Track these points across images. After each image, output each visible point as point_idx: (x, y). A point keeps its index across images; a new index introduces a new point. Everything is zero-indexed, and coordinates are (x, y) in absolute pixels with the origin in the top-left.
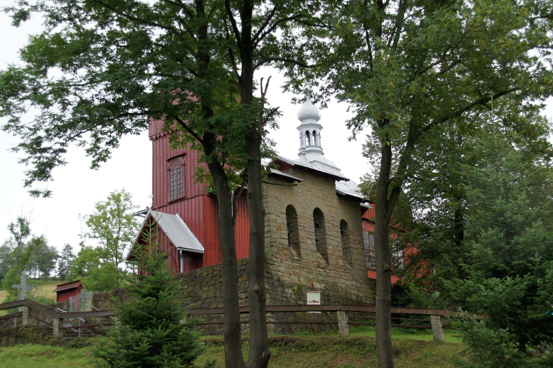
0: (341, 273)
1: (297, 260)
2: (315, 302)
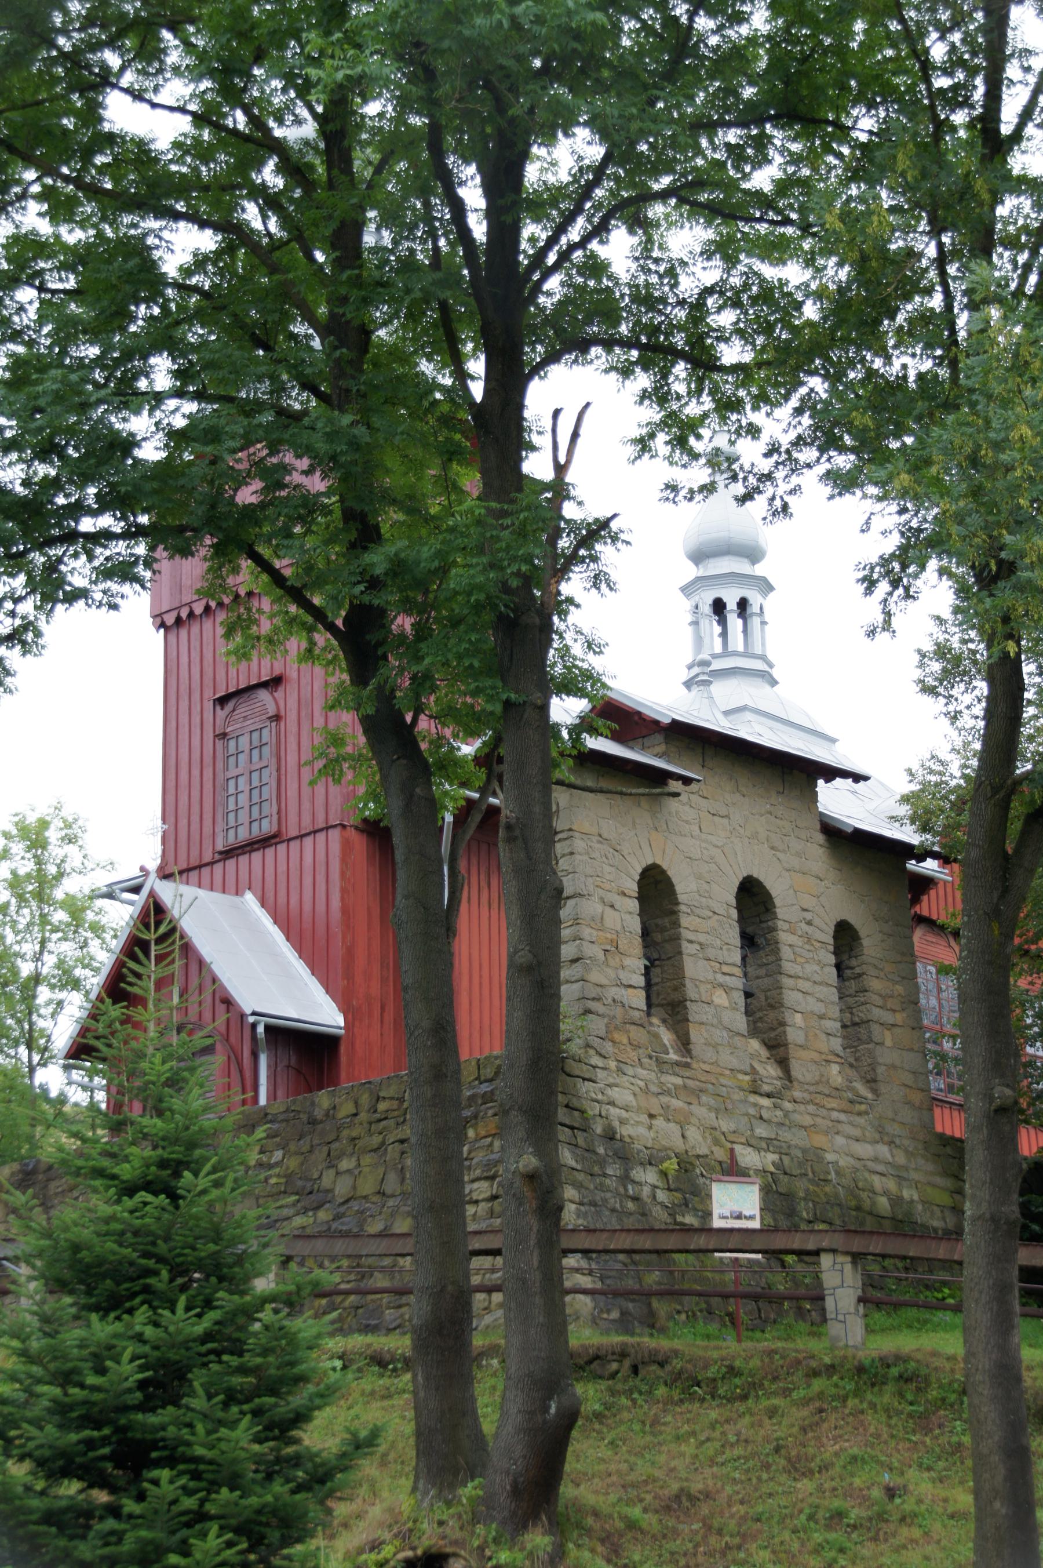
2: (739, 1217)
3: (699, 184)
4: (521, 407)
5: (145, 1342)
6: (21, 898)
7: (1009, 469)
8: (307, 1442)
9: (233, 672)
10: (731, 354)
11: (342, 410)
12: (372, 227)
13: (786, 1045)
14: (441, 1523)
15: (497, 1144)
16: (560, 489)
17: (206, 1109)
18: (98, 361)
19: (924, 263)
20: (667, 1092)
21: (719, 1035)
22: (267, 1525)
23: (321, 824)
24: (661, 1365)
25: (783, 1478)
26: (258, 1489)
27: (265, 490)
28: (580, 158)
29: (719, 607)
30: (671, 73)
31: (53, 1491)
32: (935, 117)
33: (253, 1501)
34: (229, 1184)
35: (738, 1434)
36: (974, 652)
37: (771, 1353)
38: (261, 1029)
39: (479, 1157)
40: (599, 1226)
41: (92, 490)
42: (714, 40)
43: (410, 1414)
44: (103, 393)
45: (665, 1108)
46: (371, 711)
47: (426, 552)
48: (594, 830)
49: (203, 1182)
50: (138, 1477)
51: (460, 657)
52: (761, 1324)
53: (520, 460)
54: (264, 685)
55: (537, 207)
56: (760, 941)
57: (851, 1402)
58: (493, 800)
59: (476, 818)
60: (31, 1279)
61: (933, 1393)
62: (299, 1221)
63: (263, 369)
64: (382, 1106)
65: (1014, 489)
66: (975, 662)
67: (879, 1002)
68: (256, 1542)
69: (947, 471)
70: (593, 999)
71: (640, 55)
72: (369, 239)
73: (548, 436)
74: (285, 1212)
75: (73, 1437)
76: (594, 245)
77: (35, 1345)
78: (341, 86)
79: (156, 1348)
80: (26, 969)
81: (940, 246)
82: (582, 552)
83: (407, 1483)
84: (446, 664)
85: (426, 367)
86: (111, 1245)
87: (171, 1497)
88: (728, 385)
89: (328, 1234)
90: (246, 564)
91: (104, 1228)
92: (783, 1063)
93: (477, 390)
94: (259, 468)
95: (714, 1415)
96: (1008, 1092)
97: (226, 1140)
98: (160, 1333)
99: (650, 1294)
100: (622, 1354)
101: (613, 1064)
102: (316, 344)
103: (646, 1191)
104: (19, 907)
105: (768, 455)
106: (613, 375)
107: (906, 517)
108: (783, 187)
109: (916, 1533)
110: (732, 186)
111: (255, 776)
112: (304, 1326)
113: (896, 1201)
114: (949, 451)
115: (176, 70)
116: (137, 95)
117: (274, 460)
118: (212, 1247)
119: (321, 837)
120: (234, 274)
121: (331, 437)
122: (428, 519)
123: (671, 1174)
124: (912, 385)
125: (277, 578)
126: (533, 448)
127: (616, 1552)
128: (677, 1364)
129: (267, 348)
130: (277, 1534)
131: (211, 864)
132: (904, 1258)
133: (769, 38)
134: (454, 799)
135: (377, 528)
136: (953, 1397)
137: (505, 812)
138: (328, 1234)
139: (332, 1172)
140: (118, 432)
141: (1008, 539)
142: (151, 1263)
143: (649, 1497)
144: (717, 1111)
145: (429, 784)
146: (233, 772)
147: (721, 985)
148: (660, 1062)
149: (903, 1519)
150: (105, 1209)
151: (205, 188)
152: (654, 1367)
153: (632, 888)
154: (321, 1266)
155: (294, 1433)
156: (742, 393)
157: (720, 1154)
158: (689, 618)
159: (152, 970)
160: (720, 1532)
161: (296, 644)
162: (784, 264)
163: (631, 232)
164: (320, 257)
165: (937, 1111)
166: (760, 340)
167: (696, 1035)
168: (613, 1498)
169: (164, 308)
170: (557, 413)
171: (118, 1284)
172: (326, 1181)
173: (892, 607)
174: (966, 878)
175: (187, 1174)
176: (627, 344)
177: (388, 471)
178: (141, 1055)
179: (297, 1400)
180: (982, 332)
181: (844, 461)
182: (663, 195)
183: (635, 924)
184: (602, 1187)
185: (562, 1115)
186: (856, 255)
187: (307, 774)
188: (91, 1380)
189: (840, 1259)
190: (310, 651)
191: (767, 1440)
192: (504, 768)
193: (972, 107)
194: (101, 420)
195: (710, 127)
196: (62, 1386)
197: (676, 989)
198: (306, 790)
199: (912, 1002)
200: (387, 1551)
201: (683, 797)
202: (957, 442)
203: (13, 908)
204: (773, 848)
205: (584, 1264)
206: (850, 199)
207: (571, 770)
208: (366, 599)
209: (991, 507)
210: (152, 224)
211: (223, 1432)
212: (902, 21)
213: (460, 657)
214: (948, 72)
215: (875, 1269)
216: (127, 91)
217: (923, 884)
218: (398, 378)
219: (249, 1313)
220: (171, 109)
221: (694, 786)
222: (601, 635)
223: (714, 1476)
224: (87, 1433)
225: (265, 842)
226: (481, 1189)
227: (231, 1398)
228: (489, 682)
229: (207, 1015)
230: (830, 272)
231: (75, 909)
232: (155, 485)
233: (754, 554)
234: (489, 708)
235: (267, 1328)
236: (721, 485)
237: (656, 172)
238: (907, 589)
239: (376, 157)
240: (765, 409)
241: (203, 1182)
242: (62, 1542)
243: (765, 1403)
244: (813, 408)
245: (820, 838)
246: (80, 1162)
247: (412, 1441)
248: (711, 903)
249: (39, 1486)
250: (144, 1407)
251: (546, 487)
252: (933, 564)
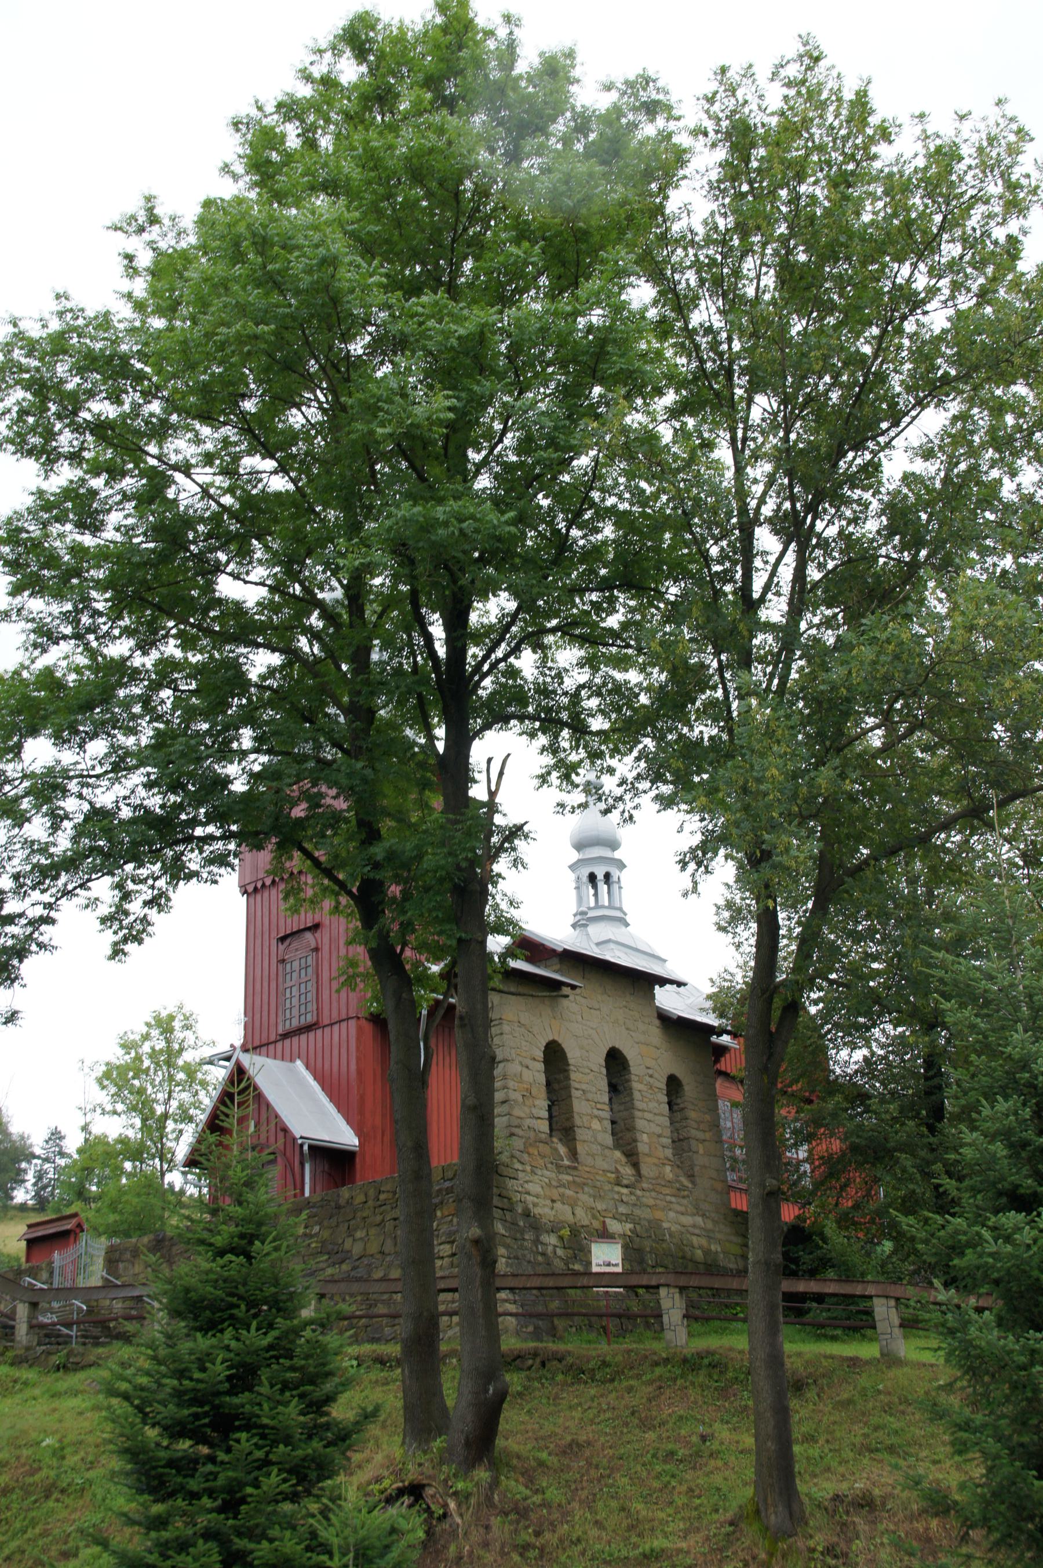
2: (609, 1264)
3: (575, 624)
4: (467, 756)
5: (230, 1351)
6: (157, 1064)
7: (766, 794)
8: (334, 1414)
9: (289, 920)
10: (597, 724)
11: (357, 759)
12: (377, 649)
13: (637, 1154)
14: (420, 1465)
15: (455, 1220)
16: (492, 806)
17: (269, 1201)
18: (208, 732)
19: (711, 671)
20: (564, 1186)
21: (595, 1148)
22: (309, 1468)
23: (344, 1016)
24: (560, 1361)
25: (637, 1431)
26: (303, 1445)
27: (309, 809)
28: (503, 609)
29: (592, 878)
30: (556, 561)
31: (174, 1446)
32: (714, 587)
33: (300, 1453)
34: (284, 1249)
35: (609, 1404)
36: (749, 905)
37: (629, 1351)
38: (306, 1148)
39: (444, 1228)
40: (520, 1272)
41: (202, 810)
42: (581, 542)
43: (400, 1395)
44: (210, 751)
45: (562, 1195)
46: (374, 945)
47: (409, 846)
48: (516, 1019)
49: (267, 1248)
50: (226, 1438)
51: (430, 911)
52: (623, 1333)
53: (467, 789)
54: (308, 929)
55: (477, 637)
56: (621, 1088)
57: (679, 1382)
58: (451, 1000)
59: (441, 1012)
60: (160, 1310)
61: (730, 1375)
62: (330, 1271)
63: (309, 735)
64: (382, 1197)
65: (769, 807)
66: (750, 912)
67: (695, 1125)
68: (302, 1479)
69: (729, 795)
71: (538, 550)
72: (375, 656)
73: (485, 774)
74: (322, 1265)
75: (186, 1412)
76: (512, 660)
77: (162, 1352)
78: (357, 569)
79: (238, 1355)
80: (159, 1109)
81: (720, 662)
82: (506, 845)
83: (398, 1439)
84: (422, 915)
85: (409, 732)
86: (209, 1289)
87: (247, 1451)
88: (595, 743)
89: (348, 1279)
90: (297, 854)
91: (205, 1277)
92: (636, 1165)
93: (440, 746)
94: (305, 795)
95: (593, 1392)
96: (774, 1182)
97: (282, 1218)
98: (240, 1345)
99: (553, 1315)
100: (535, 1354)
101: (528, 1168)
102: (342, 719)
103: (550, 1249)
104: (156, 1071)
105: (620, 785)
106: (524, 737)
107: (705, 823)
108: (625, 626)
109: (720, 1463)
110: (596, 625)
111: (303, 986)
112: (332, 1339)
113: (707, 1252)
114: (729, 783)
115: (260, 562)
116: (236, 577)
117: (315, 790)
118: (273, 1290)
119: (344, 1025)
120: (292, 678)
121: (350, 775)
122: (410, 825)
123: (566, 1238)
124: (706, 743)
125: (316, 862)
126: (476, 782)
127: (531, 1482)
128: (570, 1360)
129: (311, 722)
130: (315, 1474)
131: (275, 1042)
132: (712, 1289)
133: (614, 541)
134: (427, 1000)
135: (378, 831)
136: (742, 1376)
137: (459, 1008)
138: (348, 1279)
139: (350, 1240)
140: (219, 775)
141: (767, 837)
142: (235, 1300)
143: (552, 1446)
144: (595, 1197)
145: (411, 991)
146: (288, 984)
148: (558, 1166)
149: (711, 1455)
150: (205, 1265)
151: (276, 628)
152: (555, 1362)
153: (540, 1055)
154: (344, 1300)
155: (325, 1409)
156: (603, 747)
157: (596, 1224)
158: (574, 885)
159: (236, 1112)
160: (597, 1467)
161: (328, 903)
162: (627, 671)
163: (534, 652)
164: (344, 667)
165: (732, 1194)
166: (614, 716)
167: (580, 1148)
168: (529, 1446)
169: (249, 699)
170: (489, 760)
171: (214, 1313)
172: (347, 1245)
173: (698, 878)
174: (747, 1047)
175: (257, 1242)
176: (533, 718)
177: (385, 796)
178: (228, 1166)
179: (328, 1387)
180: (747, 711)
181: (666, 789)
182: (553, 631)
183: (542, 1078)
184: (521, 1247)
185: (496, 1201)
186: (670, 666)
187: (335, 985)
188: (197, 1375)
189: (672, 1290)
190: (336, 907)
191: (626, 1407)
192: (458, 980)
193: (735, 582)
194: (209, 767)
195: (581, 592)
196: (179, 1379)
197: (568, 1119)
198: (335, 996)
199: (715, 1126)
200: (386, 1483)
201: (571, 998)
202: (734, 778)
203: (152, 1071)
205: (511, 1297)
206: (665, 634)
207: (500, 981)
208: (371, 875)
209: (756, 817)
210: (243, 650)
211: (280, 1408)
212: (692, 533)
213: (430, 911)
214: (719, 563)
215: (694, 1296)
216: (230, 574)
217: (721, 1051)
218: (392, 739)
219: (296, 1332)
220: (256, 584)
221: (578, 991)
222: (518, 897)
223: (593, 1431)
224: (194, 1409)
225: (308, 1028)
226: (446, 1249)
227: (286, 1386)
228: (447, 927)
229: (272, 1139)
230: (655, 676)
231: (190, 1071)
232: (241, 806)
233: (614, 845)
234: (449, 943)
235: (308, 1341)
236: (591, 803)
237: (549, 618)
238: (706, 867)
239: (379, 609)
240: (618, 757)
241: (267, 1248)
242: (179, 1479)
243: (625, 1384)
244: (647, 757)
245: (657, 1022)
246: (190, 1235)
247: (401, 1412)
249: (165, 1443)
250: (229, 1393)
251: (483, 804)
252: (722, 852)
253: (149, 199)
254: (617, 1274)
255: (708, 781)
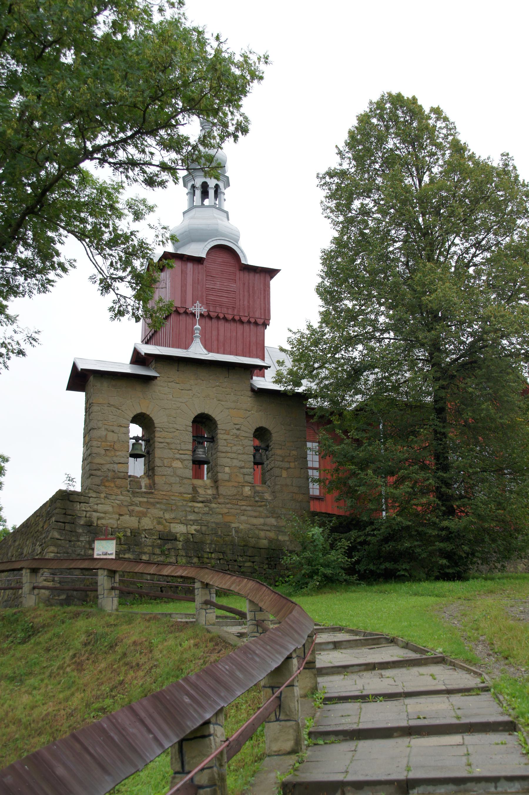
0: (244, 507)
1: (145, 493)
2: (106, 554)
70: (95, 470)
147: (178, 459)
204: (219, 400)
245: (250, 393)
248: (175, 426)
253: (337, 146)
254: (112, 559)
255: (389, 245)
